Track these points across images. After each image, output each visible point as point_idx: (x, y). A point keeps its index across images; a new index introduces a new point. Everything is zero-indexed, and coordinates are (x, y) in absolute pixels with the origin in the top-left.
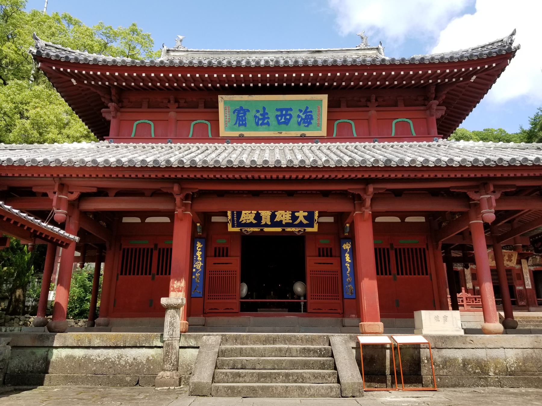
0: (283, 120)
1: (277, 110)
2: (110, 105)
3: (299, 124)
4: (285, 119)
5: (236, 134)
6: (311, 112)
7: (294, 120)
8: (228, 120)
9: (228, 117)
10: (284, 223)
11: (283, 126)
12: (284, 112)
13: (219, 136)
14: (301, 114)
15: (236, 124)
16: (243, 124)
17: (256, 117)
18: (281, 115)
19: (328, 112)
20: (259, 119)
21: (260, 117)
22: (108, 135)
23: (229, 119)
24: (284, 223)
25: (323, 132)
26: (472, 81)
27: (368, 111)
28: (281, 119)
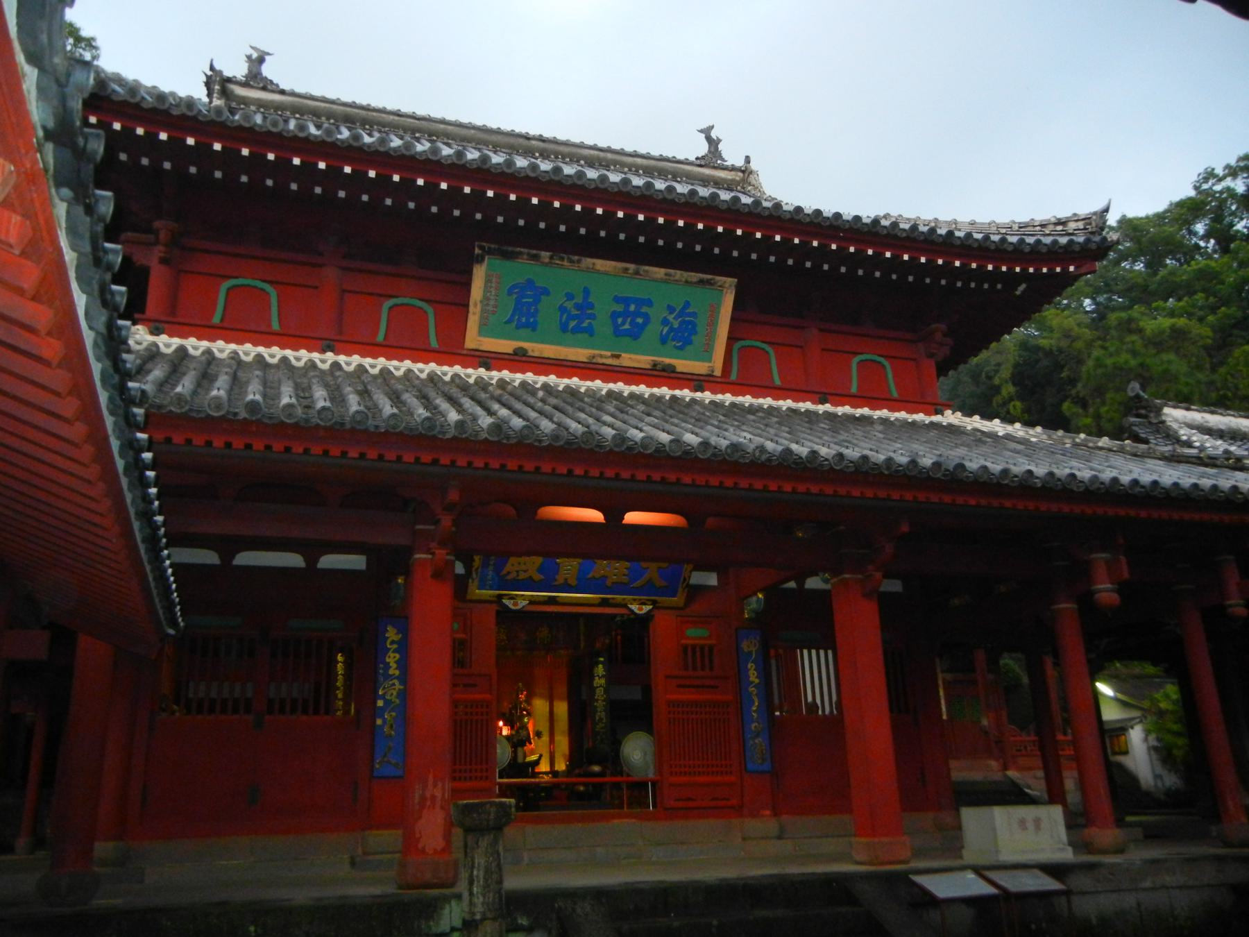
0: (627, 326)
1: (617, 300)
2: (157, 224)
3: (664, 340)
4: (633, 323)
5: (505, 346)
6: (694, 314)
7: (653, 330)
8: (490, 308)
9: (492, 303)
10: (609, 583)
11: (627, 340)
12: (632, 308)
13: (463, 348)
14: (671, 318)
15: (509, 321)
16: (527, 325)
17: (562, 309)
18: (626, 314)
19: (733, 319)
20: (571, 317)
21: (575, 312)
22: (143, 312)
23: (495, 306)
24: (609, 583)
25: (717, 364)
26: (1018, 293)
27: (320, 266)
28: (623, 323)
